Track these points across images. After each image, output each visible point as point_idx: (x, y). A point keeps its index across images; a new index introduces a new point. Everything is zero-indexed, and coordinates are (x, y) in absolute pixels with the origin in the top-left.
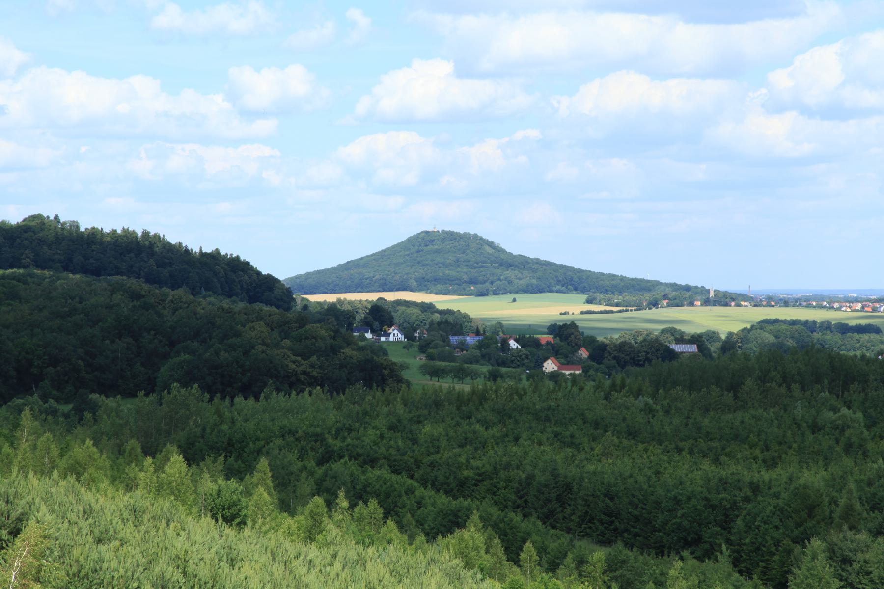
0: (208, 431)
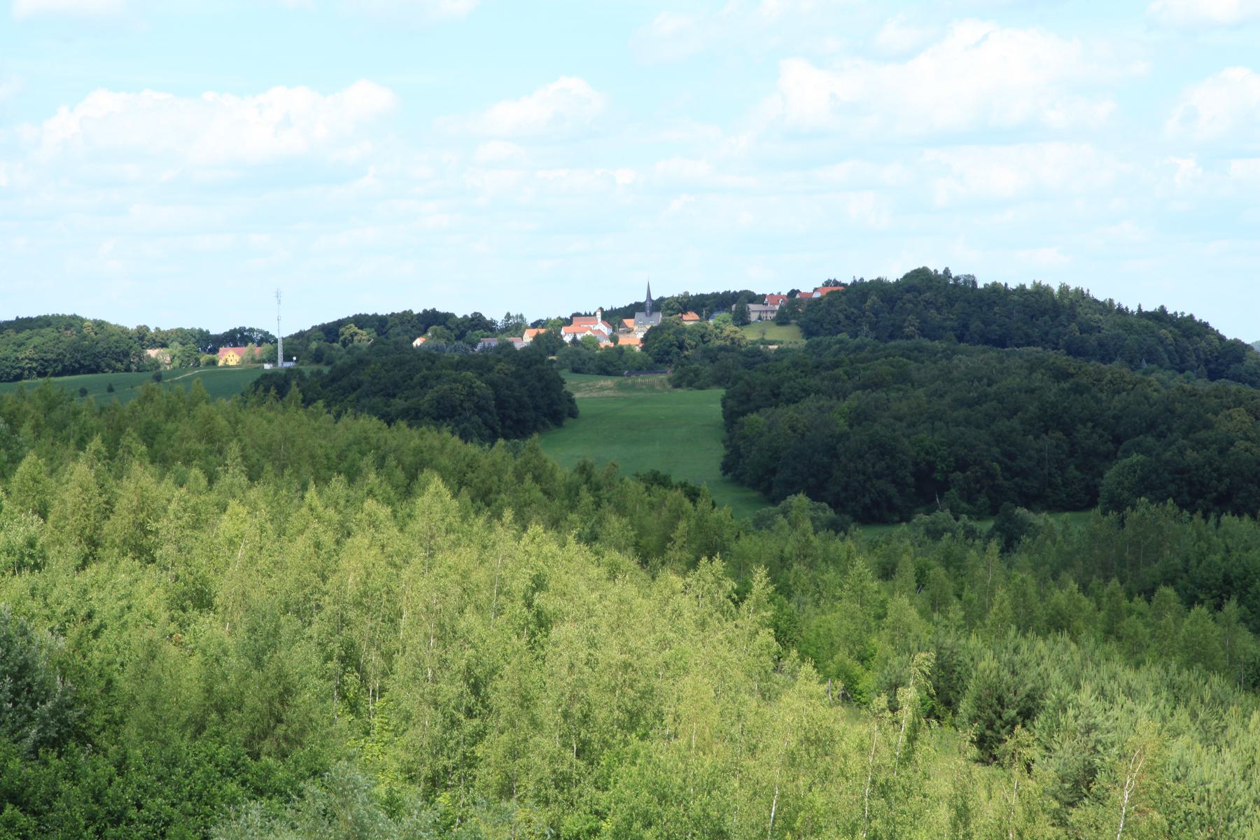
0: (1193, 562)
